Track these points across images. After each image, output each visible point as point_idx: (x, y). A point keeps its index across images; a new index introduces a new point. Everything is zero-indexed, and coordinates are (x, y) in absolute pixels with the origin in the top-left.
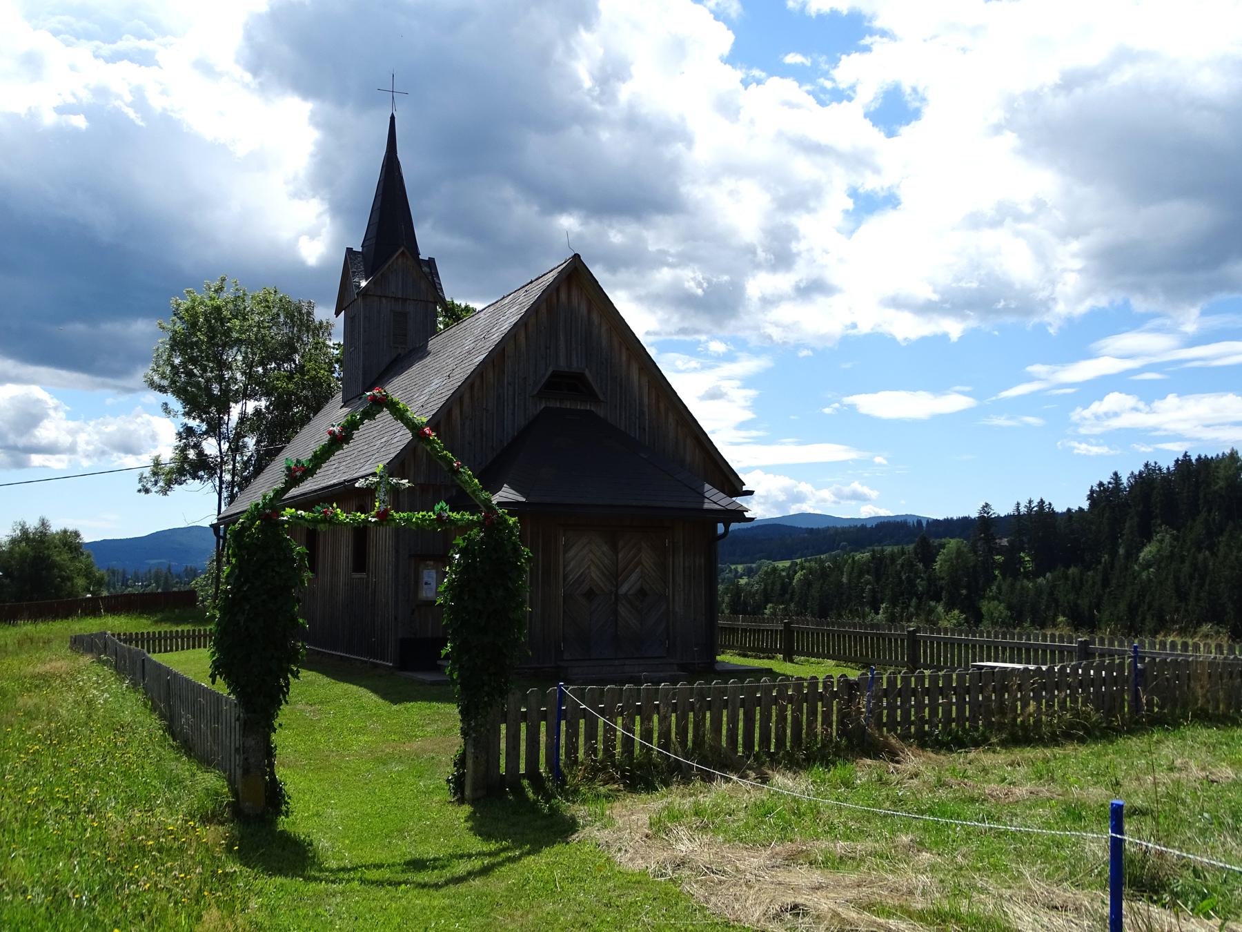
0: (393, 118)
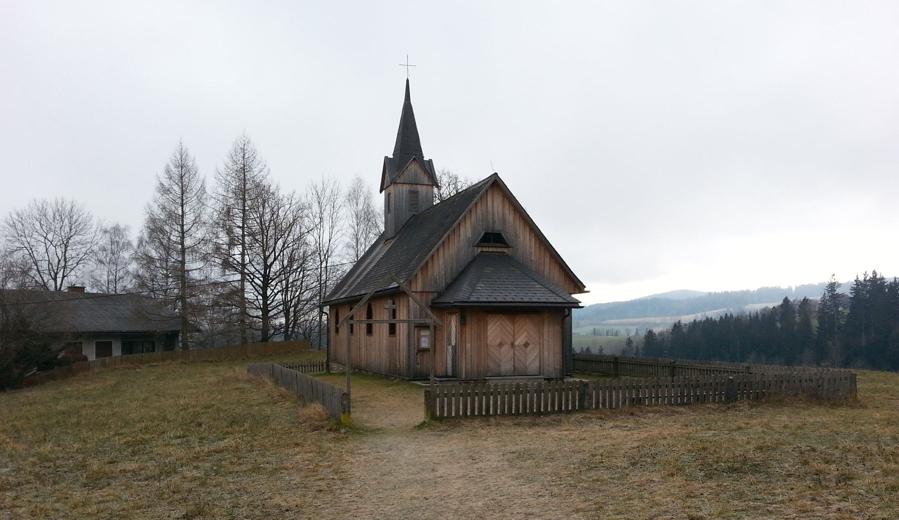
0: (408, 81)
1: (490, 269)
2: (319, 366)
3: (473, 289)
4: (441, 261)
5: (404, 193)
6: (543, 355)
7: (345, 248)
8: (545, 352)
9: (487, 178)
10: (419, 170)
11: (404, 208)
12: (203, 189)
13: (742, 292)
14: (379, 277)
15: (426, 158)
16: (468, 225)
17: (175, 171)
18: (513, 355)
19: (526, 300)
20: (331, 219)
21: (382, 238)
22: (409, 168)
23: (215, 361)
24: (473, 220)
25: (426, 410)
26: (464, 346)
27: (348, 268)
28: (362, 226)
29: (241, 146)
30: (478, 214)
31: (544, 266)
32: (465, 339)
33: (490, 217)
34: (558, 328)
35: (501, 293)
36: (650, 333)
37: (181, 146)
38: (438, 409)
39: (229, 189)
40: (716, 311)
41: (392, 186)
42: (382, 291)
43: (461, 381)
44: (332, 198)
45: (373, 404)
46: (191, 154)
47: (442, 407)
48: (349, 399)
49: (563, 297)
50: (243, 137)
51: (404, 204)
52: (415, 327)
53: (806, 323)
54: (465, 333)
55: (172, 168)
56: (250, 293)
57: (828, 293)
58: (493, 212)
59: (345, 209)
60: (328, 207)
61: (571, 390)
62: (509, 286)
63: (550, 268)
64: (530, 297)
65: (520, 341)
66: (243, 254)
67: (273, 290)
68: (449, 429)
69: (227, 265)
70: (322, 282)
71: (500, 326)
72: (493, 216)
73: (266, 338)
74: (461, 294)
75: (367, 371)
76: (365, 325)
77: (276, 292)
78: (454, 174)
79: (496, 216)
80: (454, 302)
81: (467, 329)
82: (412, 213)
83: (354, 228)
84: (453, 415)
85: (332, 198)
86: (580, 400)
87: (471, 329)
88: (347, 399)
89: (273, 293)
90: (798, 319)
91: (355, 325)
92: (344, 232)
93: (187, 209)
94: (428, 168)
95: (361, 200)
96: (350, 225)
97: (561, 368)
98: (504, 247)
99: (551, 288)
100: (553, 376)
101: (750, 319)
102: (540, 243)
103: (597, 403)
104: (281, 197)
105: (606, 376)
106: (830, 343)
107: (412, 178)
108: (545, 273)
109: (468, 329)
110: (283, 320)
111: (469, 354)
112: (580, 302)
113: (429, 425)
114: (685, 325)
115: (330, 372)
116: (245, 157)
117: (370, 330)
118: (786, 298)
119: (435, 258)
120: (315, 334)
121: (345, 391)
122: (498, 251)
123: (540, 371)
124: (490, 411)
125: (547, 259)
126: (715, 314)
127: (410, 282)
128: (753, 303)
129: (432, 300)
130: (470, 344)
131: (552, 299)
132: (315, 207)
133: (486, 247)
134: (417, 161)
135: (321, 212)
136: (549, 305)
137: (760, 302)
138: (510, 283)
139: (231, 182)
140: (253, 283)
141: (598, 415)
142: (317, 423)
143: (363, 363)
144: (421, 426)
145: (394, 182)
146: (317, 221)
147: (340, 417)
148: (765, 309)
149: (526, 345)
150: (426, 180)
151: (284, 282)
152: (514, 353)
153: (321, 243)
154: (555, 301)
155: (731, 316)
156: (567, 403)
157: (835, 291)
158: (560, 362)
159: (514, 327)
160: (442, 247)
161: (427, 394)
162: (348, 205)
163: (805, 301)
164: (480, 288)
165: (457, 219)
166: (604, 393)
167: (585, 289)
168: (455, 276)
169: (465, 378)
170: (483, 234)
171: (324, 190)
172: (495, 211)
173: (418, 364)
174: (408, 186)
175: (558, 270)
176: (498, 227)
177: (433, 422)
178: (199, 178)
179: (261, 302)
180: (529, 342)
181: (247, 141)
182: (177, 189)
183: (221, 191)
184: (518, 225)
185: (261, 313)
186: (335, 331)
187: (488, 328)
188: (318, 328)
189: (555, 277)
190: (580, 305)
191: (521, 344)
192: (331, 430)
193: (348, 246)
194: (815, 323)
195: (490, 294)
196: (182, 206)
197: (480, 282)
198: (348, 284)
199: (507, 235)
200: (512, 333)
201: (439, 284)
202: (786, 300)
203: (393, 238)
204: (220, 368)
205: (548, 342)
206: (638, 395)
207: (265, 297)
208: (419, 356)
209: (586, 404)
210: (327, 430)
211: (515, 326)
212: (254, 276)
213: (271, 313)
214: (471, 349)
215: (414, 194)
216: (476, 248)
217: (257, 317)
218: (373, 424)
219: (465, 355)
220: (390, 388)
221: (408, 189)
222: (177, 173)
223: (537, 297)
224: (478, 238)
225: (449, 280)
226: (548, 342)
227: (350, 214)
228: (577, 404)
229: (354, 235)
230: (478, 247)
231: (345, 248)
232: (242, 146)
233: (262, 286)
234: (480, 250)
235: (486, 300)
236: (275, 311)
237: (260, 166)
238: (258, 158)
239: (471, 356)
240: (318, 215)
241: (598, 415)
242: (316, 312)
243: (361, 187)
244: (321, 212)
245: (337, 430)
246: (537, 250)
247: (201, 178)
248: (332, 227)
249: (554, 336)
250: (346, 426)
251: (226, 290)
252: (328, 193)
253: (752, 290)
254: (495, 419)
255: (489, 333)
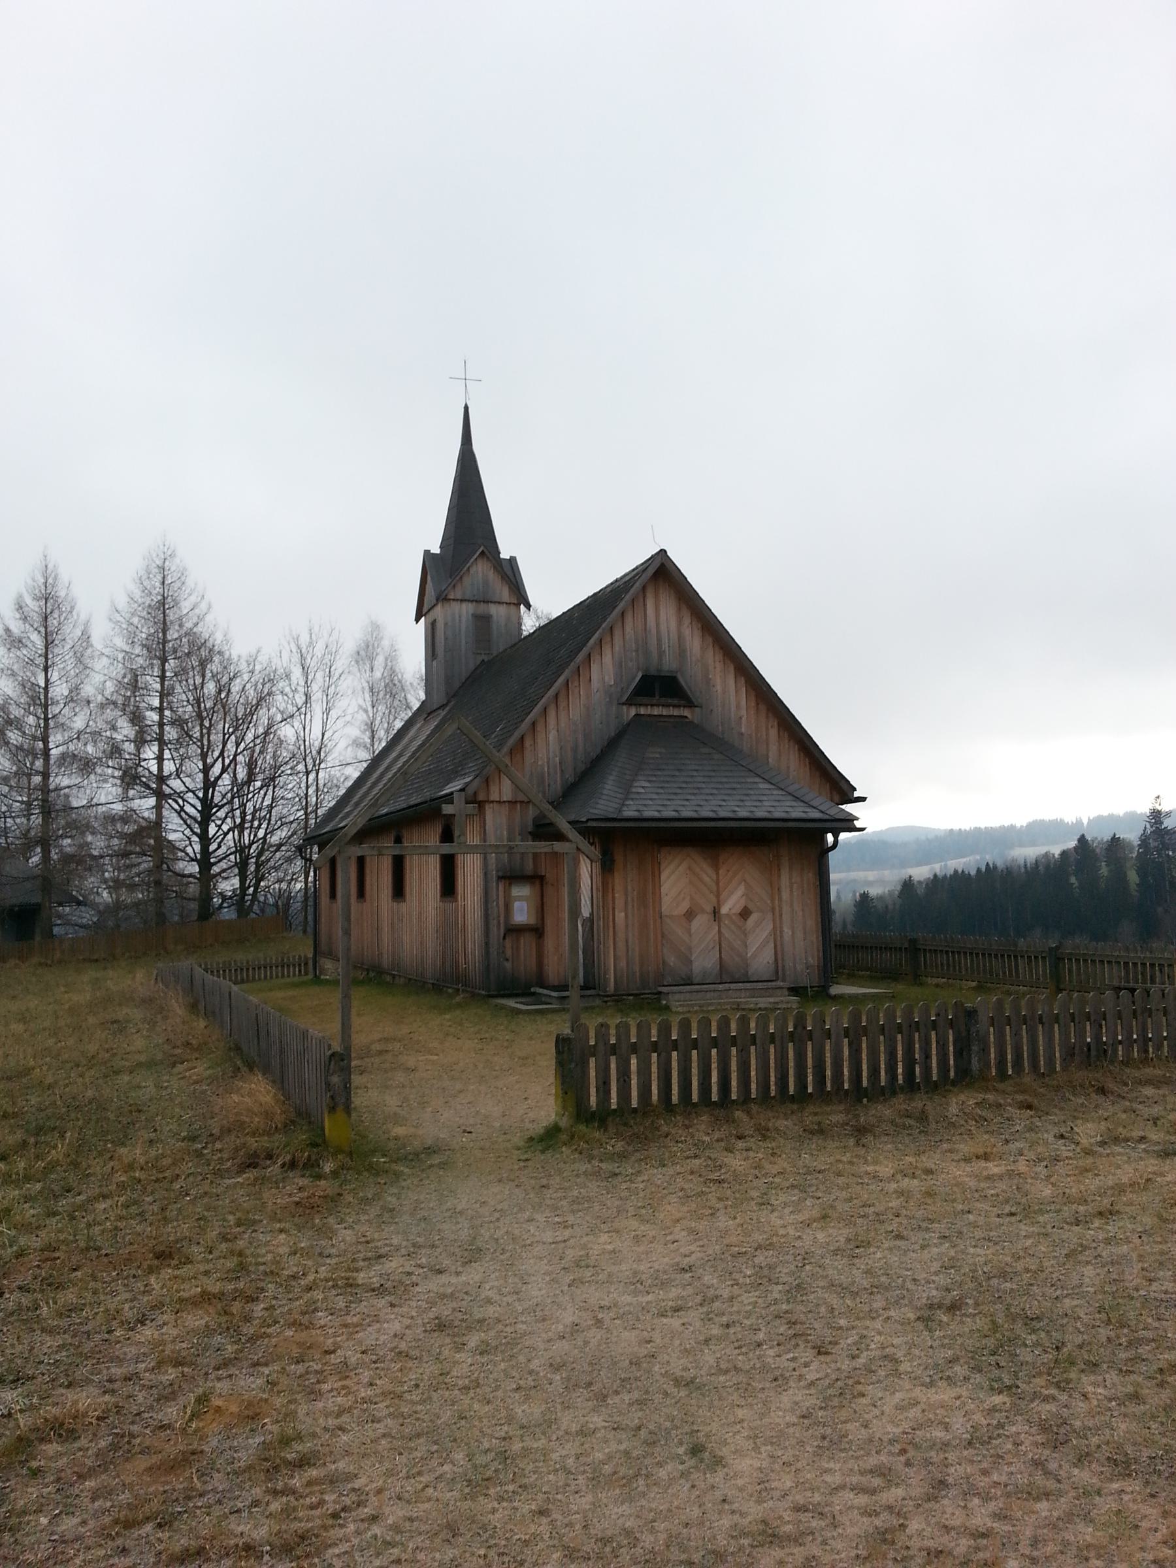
0: (466, 408)
1: (659, 750)
2: (300, 965)
3: (627, 793)
4: (552, 735)
5: (464, 619)
6: (782, 937)
7: (350, 749)
8: (785, 930)
9: (643, 564)
10: (492, 575)
11: (463, 648)
12: (86, 637)
13: (1002, 828)
14: (415, 779)
15: (505, 554)
16: (608, 658)
17: (33, 605)
18: (717, 938)
19: (743, 813)
20: (325, 697)
21: (425, 711)
22: (472, 571)
23: (104, 959)
24: (617, 648)
25: (560, 1092)
26: (611, 917)
27: (354, 773)
28: (381, 708)
29: (158, 563)
30: (627, 637)
31: (767, 745)
32: (614, 903)
33: (653, 641)
34: (810, 876)
35: (687, 800)
36: (865, 896)
37: (46, 560)
38: (593, 1091)
39: (136, 640)
40: (964, 860)
41: (439, 605)
42: (425, 802)
43: (608, 996)
44: (328, 657)
45: (411, 1062)
46: (64, 575)
47: (604, 1083)
48: (346, 1071)
49: (820, 808)
50: (162, 547)
51: (463, 642)
52: (500, 878)
53: (1119, 876)
54: (613, 890)
55: (29, 601)
56: (176, 831)
57: (1152, 827)
58: (658, 632)
59: (350, 677)
60: (319, 675)
61: (934, 1028)
62: (704, 786)
63: (779, 751)
64: (749, 809)
65: (731, 904)
66: (160, 759)
67: (219, 827)
68: (631, 1148)
69: (130, 778)
70: (309, 810)
71: (688, 872)
72: (659, 640)
73: (206, 911)
74: (604, 797)
75: (394, 976)
76: (390, 858)
77: (225, 830)
78: (545, 612)
79: (665, 640)
80: (588, 820)
81: (617, 881)
82: (480, 659)
83: (366, 711)
84: (634, 1104)
85: (328, 657)
86: (959, 1054)
87: (625, 882)
88: (342, 1070)
89: (221, 832)
90: (1104, 871)
91: (368, 860)
92: (348, 718)
93: (54, 675)
94: (509, 573)
95: (379, 661)
96: (360, 707)
97: (822, 964)
98: (684, 707)
99: (791, 789)
100: (804, 981)
101: (1026, 871)
102: (757, 696)
103: (1002, 1063)
104: (234, 657)
105: (889, 978)
106: (1160, 909)
107: (478, 589)
108: (770, 760)
109: (618, 879)
110: (236, 882)
111: (621, 935)
112: (857, 819)
113: (572, 1137)
114: (920, 882)
115: (319, 978)
116: (166, 582)
117: (399, 891)
118: (1083, 836)
119: (540, 727)
120: (297, 906)
121: (337, 1047)
122: (671, 713)
123: (777, 972)
124: (730, 1092)
125: (773, 732)
126: (967, 863)
127: (487, 781)
128: (1021, 845)
129: (534, 820)
130: (623, 914)
131: (798, 812)
132: (297, 674)
133: (646, 705)
134: (488, 558)
135: (306, 682)
136: (790, 824)
137: (1033, 843)
138: (705, 780)
139: (139, 626)
140: (183, 814)
141: (1020, 1098)
142: (253, 1143)
143: (386, 962)
144: (549, 1138)
145: (442, 598)
146: (300, 699)
147: (323, 1121)
148: (1046, 855)
149: (745, 914)
150: (505, 594)
151: (237, 813)
152: (719, 931)
153: (307, 739)
154: (803, 816)
155: (995, 867)
156: (926, 1062)
157: (1162, 823)
158: (818, 951)
159: (717, 874)
160: (553, 706)
161: (562, 1044)
162: (355, 669)
163: (1115, 840)
164: (643, 791)
165: (585, 645)
166: (1017, 1034)
167: (856, 794)
168: (582, 767)
169: (616, 989)
170: (638, 679)
171: (311, 644)
172: (663, 627)
173: (507, 960)
174: (470, 605)
175: (797, 755)
176: (669, 664)
177: (582, 1128)
178: (78, 619)
179: (197, 847)
180: (751, 906)
181: (169, 553)
182: (37, 640)
183: (120, 642)
184: (710, 661)
185: (197, 869)
186: (328, 896)
187: (663, 877)
188: (302, 893)
189: (792, 769)
190: (858, 824)
191: (734, 911)
192: (293, 1165)
193: (356, 743)
194: (1133, 877)
195: (665, 803)
196: (46, 669)
197: (640, 778)
198: (355, 799)
199: (690, 679)
200: (714, 888)
201: (549, 785)
202: (1082, 840)
203: (443, 707)
204: (111, 973)
205: (792, 905)
206: (1097, 1037)
207: (205, 839)
208: (508, 943)
209: (975, 1064)
210: (283, 1166)
211: (720, 872)
212: (184, 800)
213: (216, 869)
214: (627, 926)
215: (483, 622)
216: (625, 707)
217: (191, 875)
218: (412, 1130)
219: (614, 939)
220: (447, 1017)
221: (471, 611)
222: (37, 609)
223: (764, 809)
224: (628, 688)
225: (570, 778)
226: (792, 905)
227: (359, 688)
228: (952, 1062)
229: (367, 724)
230: (631, 705)
231: (350, 749)
232: (159, 563)
233: (199, 819)
234: (633, 711)
235: (656, 815)
236: (223, 865)
237: (193, 599)
238: (190, 583)
239: (627, 941)
240: (301, 690)
241: (1020, 1098)
242: (153, 728)
243: (379, 639)
244: (306, 682)
245: (311, 1167)
246: (752, 712)
247: (83, 617)
248: (327, 711)
249: (803, 893)
250: (339, 1150)
251: (129, 829)
252: (319, 649)
253: (1018, 825)
254: (748, 1113)
255: (664, 889)
